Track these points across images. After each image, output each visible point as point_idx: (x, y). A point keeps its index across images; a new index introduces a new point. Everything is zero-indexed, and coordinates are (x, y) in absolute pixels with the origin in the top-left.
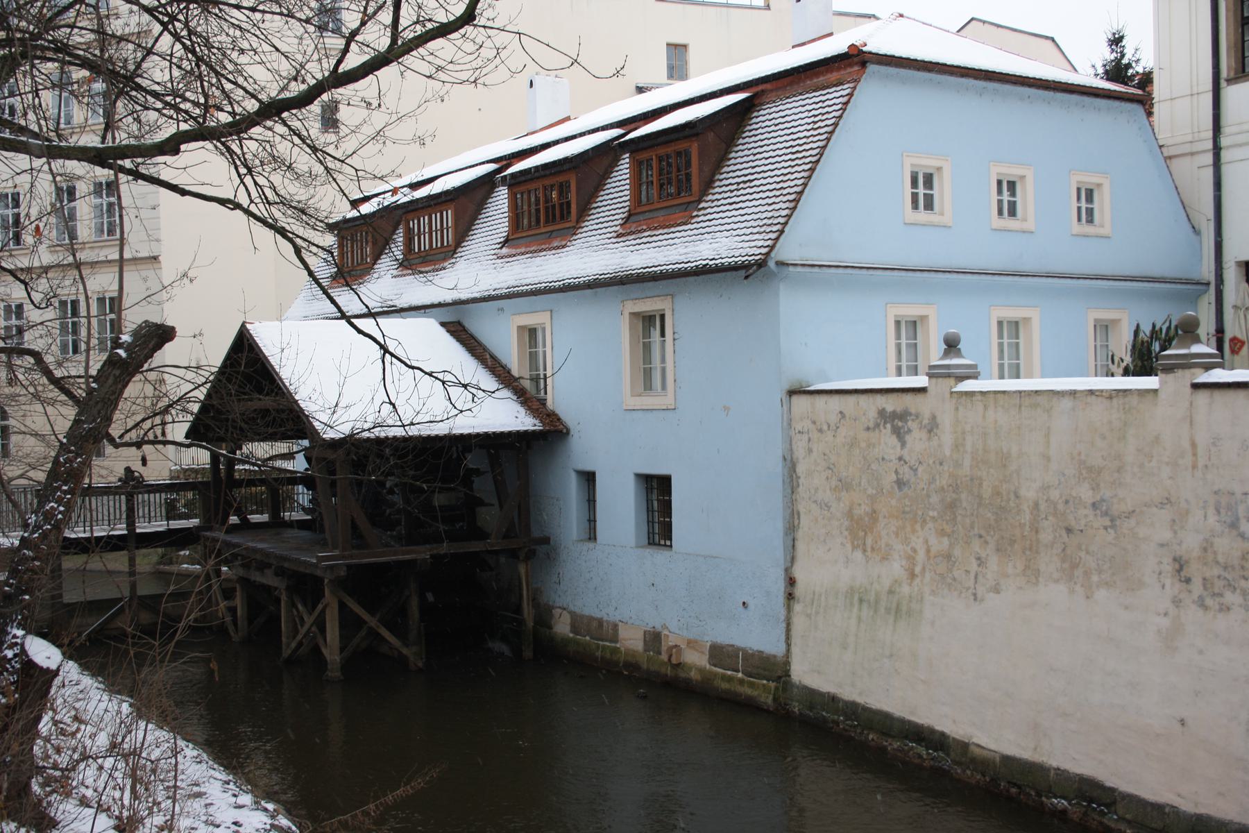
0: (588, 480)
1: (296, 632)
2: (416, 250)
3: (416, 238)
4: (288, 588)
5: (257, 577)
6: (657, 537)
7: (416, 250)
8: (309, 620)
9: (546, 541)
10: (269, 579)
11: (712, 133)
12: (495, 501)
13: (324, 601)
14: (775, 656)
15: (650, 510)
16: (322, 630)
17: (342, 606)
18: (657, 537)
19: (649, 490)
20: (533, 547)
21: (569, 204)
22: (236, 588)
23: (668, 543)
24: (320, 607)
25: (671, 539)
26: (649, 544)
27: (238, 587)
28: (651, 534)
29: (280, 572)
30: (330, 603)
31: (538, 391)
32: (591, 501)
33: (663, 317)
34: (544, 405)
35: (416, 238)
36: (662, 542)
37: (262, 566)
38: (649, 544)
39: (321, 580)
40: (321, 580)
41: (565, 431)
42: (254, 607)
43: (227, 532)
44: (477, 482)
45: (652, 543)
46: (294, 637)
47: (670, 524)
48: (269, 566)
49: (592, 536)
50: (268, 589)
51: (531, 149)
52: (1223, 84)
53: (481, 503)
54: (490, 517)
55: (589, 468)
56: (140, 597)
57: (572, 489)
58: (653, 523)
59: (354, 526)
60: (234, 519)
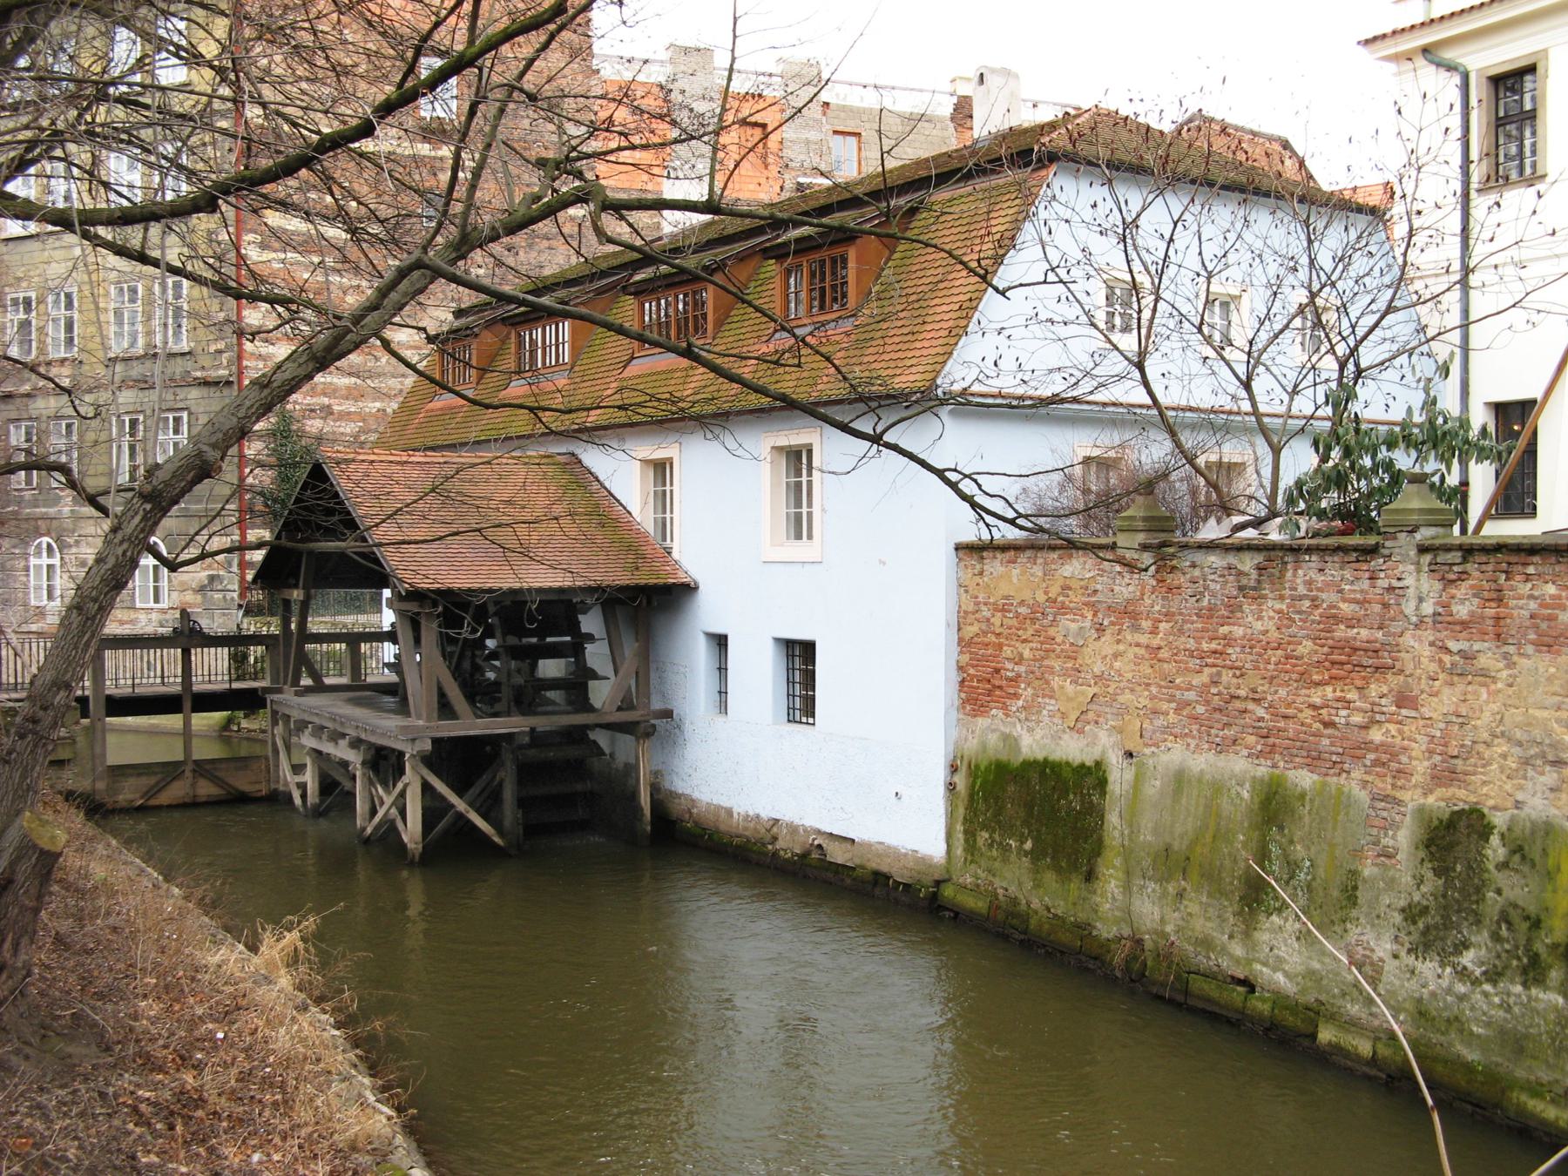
0: (719, 645)
1: (373, 812)
2: (540, 365)
3: (539, 351)
4: (364, 763)
5: (328, 748)
6: (797, 712)
7: (540, 365)
8: (388, 800)
9: (668, 714)
10: (342, 751)
11: (711, 288)
12: (611, 674)
13: (405, 779)
14: (931, 858)
15: (790, 682)
16: (403, 813)
17: (426, 788)
18: (797, 712)
19: (790, 656)
20: (653, 722)
21: (704, 316)
22: (305, 765)
23: (811, 721)
24: (400, 786)
25: (813, 716)
26: (789, 721)
27: (308, 761)
28: (791, 709)
29: (356, 744)
30: (412, 779)
31: (664, 539)
32: (722, 670)
33: (810, 452)
34: (669, 553)
35: (539, 351)
36: (804, 720)
37: (336, 736)
38: (789, 721)
39: (401, 754)
40: (401, 754)
41: (692, 584)
42: (328, 786)
43: (297, 694)
44: (590, 648)
45: (791, 720)
46: (370, 820)
47: (813, 698)
48: (343, 735)
49: (723, 707)
50: (344, 764)
51: (1468, 394)
52: (1473, 194)
53: (594, 676)
54: (601, 694)
55: (719, 629)
56: (195, 762)
57: (700, 655)
58: (794, 709)
59: (442, 695)
60: (306, 681)
